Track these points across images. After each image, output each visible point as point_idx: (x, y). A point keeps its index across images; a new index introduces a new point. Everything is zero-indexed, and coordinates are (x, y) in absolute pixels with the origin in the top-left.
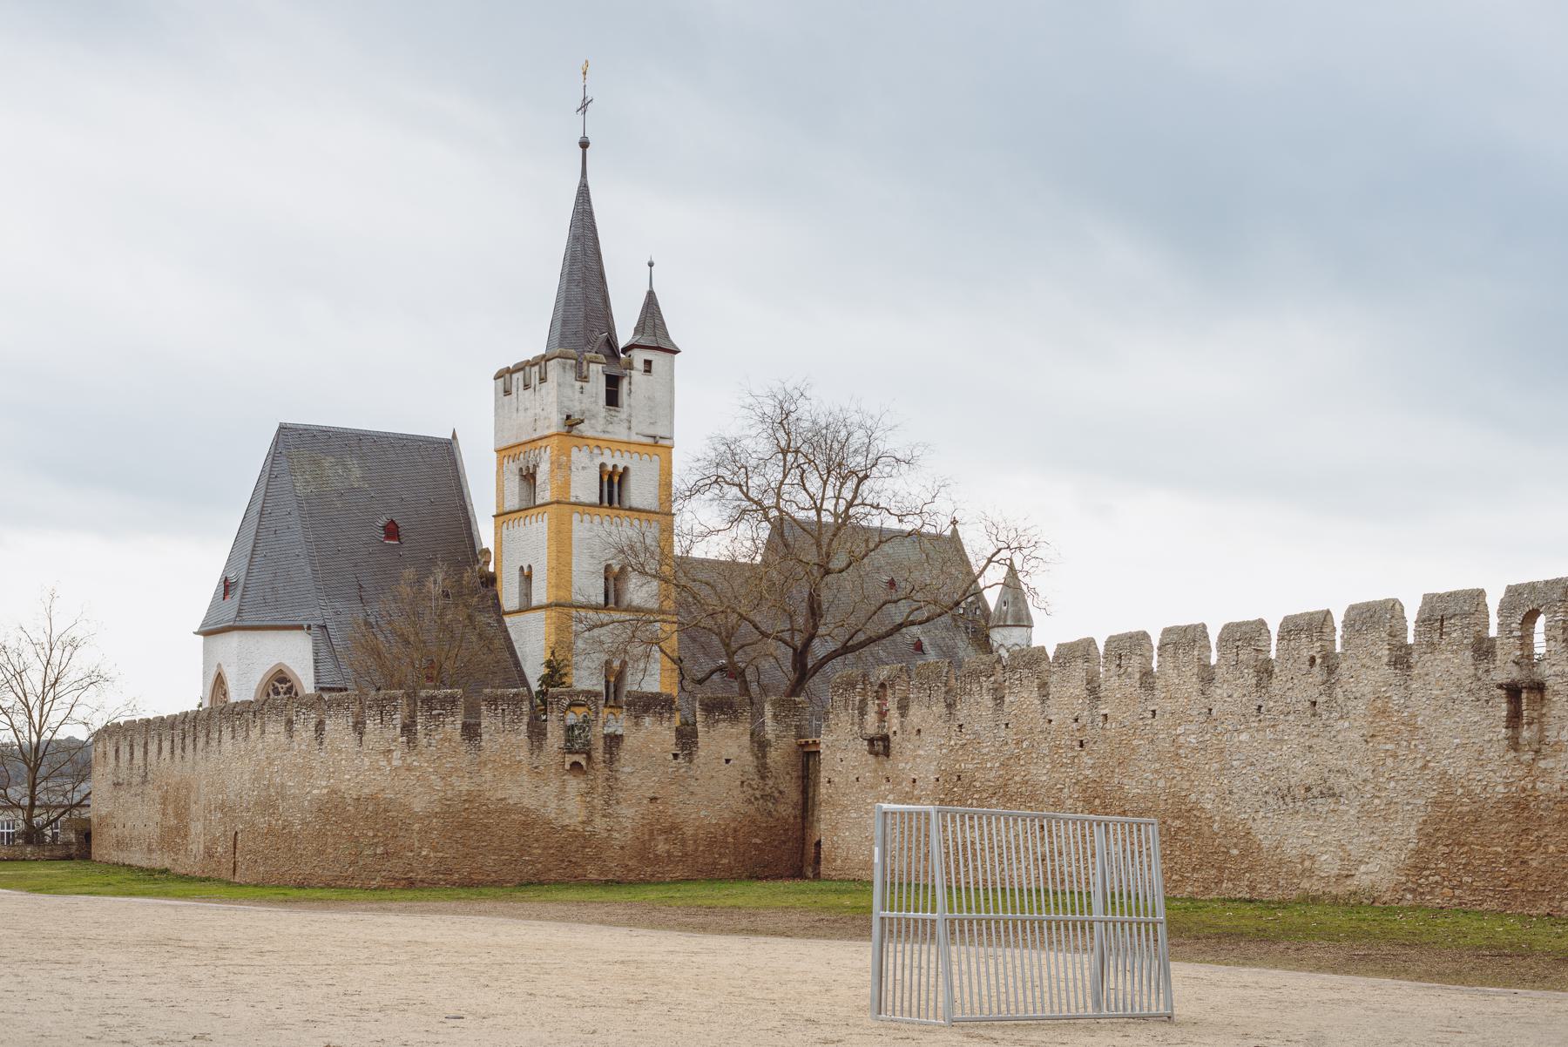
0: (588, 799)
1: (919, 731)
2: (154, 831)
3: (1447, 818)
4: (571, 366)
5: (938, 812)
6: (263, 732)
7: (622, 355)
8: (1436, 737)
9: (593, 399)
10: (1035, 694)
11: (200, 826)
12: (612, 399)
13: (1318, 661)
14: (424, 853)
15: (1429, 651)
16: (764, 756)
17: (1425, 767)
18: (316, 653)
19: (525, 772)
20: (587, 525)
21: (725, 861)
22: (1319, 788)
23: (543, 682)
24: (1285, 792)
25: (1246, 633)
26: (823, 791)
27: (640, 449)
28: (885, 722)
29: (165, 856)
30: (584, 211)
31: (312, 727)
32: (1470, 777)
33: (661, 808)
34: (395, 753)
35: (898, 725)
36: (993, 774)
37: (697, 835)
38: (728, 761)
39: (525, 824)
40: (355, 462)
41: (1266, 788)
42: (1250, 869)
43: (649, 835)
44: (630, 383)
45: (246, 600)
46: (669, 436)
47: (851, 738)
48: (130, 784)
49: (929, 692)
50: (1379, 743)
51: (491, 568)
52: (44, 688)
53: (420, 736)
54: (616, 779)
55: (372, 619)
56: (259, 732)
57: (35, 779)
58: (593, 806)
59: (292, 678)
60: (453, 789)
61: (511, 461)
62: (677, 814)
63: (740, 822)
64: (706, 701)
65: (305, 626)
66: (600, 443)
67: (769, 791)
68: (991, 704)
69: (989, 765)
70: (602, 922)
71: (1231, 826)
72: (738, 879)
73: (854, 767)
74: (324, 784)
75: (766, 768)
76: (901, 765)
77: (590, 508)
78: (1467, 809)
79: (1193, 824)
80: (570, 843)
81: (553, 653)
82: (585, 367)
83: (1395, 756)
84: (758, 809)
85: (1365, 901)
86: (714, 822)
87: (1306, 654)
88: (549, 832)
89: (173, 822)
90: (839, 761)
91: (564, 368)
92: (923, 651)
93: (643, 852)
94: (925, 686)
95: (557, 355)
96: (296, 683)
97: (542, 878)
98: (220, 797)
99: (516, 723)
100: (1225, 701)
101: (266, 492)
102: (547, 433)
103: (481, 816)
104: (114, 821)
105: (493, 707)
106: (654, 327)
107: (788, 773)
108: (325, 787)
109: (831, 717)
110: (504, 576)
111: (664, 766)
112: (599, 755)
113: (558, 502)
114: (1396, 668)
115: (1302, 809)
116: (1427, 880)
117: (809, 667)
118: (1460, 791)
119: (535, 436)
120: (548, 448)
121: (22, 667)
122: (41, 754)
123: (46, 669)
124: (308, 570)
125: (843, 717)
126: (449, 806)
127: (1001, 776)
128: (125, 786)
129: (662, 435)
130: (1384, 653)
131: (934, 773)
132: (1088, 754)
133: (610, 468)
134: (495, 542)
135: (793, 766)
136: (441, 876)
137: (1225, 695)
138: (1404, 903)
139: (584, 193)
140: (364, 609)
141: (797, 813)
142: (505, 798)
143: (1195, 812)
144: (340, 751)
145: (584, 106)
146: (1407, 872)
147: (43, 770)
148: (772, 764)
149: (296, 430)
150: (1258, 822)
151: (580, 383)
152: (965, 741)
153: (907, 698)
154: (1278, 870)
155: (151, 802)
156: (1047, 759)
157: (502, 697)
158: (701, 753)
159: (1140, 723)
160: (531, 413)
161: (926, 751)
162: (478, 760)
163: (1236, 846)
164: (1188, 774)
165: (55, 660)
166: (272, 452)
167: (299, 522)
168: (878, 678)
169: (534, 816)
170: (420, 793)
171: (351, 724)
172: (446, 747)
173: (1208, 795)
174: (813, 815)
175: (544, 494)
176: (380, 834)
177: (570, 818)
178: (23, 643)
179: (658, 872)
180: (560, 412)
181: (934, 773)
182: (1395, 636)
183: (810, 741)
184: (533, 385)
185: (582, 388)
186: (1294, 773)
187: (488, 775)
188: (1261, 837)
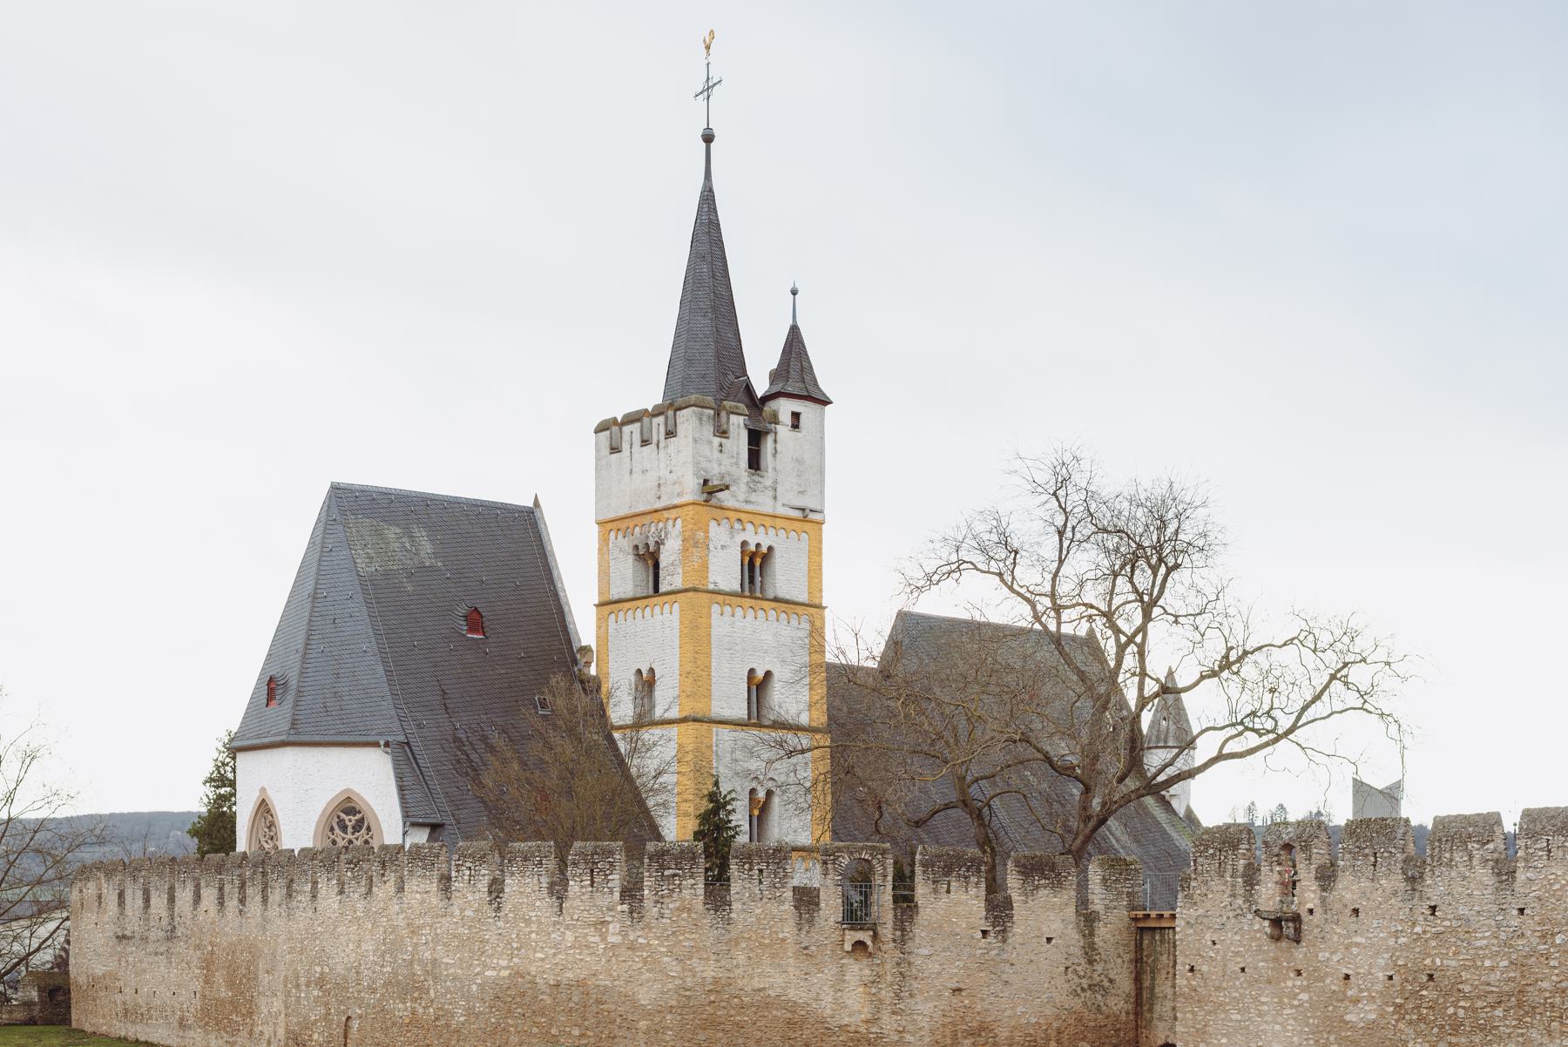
0: (874, 991)
1: (1356, 911)
9: (735, 460)
11: (277, 1005)
12: (755, 462)
16: (1092, 934)
18: (399, 778)
19: (791, 955)
20: (727, 618)
30: (710, 221)
31: (483, 885)
33: (967, 1002)
34: (611, 926)
35: (1317, 902)
37: (1012, 1038)
38: (1049, 940)
39: (790, 1023)
40: (424, 534)
44: (775, 441)
45: (302, 708)
46: (819, 508)
47: (1231, 914)
48: (145, 939)
51: (593, 671)
53: (648, 903)
54: (909, 964)
58: (880, 1000)
59: (364, 807)
63: (1064, 1020)
64: (1023, 861)
65: (382, 743)
66: (742, 516)
67: (1098, 979)
69: (1487, 963)
73: (1237, 954)
74: (504, 963)
75: (1095, 949)
77: (733, 598)
84: (1085, 1004)
86: (1034, 1020)
88: (824, 1034)
90: (1209, 943)
91: (701, 420)
94: (1367, 851)
95: (692, 403)
96: (369, 820)
98: (318, 969)
99: (778, 888)
101: (319, 570)
102: (677, 501)
103: (732, 1012)
105: (747, 866)
106: (802, 371)
107: (1119, 956)
108: (505, 968)
112: (887, 931)
119: (658, 505)
120: (679, 522)
124: (380, 670)
126: (689, 998)
128: (136, 941)
129: (813, 507)
131: (1384, 969)
139: (708, 199)
140: (450, 721)
141: (1130, 1008)
142: (764, 988)
144: (528, 922)
148: (1101, 944)
149: (351, 491)
151: (719, 439)
152: (1441, 929)
158: (1017, 930)
162: (727, 937)
166: (323, 519)
167: (364, 609)
169: (803, 1013)
170: (648, 981)
171: (545, 885)
172: (683, 919)
174: (1151, 1010)
176: (589, 1033)
177: (850, 1016)
180: (696, 475)
181: (1384, 969)
184: (655, 440)
185: (721, 445)
187: (741, 958)
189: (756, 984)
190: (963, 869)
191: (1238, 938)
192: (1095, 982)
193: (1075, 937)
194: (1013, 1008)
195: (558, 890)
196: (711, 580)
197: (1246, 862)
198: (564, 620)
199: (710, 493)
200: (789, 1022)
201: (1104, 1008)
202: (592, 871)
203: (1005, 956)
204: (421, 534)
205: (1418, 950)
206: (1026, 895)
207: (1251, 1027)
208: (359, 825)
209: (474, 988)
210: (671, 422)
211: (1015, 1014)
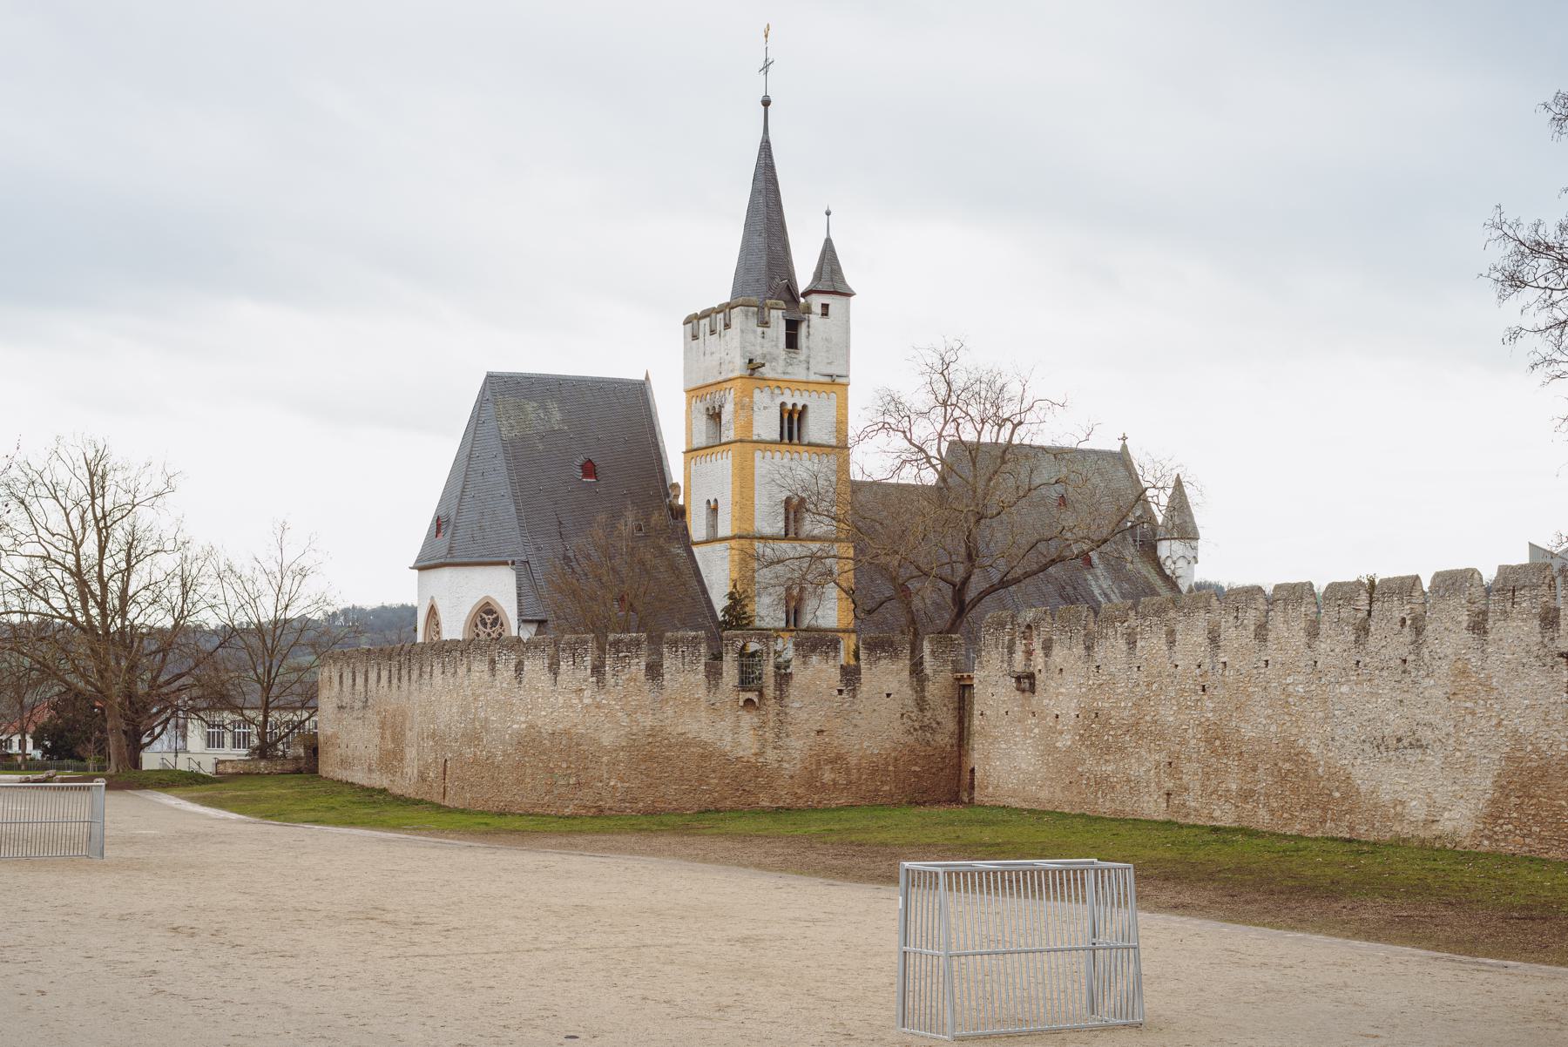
0: (760, 733)
1: (1061, 670)
2: (374, 753)
3: (1518, 772)
4: (753, 313)
5: (944, 873)
6: (469, 670)
7: (802, 300)
8: (1508, 698)
9: (774, 343)
10: (1163, 641)
12: (792, 342)
13: (1408, 622)
14: (612, 784)
15: (1503, 618)
16: (923, 690)
17: (1499, 724)
18: (519, 587)
21: (886, 788)
22: (1409, 740)
23: (726, 612)
24: (1380, 742)
25: (1346, 593)
26: (976, 722)
27: (817, 387)
28: (1031, 660)
29: (384, 777)
30: (766, 164)
32: (1538, 735)
34: (585, 692)
35: (1043, 664)
36: (1126, 713)
38: (888, 695)
41: (1362, 738)
42: (1350, 811)
43: (817, 766)
44: (808, 326)
46: (844, 374)
48: (352, 708)
49: (1069, 634)
50: (1460, 701)
51: (681, 501)
52: (276, 612)
53: (608, 676)
54: (786, 714)
55: (571, 554)
56: (465, 670)
57: (268, 698)
59: (498, 609)
60: (638, 725)
61: (698, 402)
62: (842, 745)
65: (510, 562)
66: (781, 384)
67: (928, 722)
68: (1124, 647)
70: (758, 866)
71: (1333, 770)
72: (898, 805)
74: (523, 719)
75: (925, 701)
76: (1046, 702)
78: (1536, 764)
79: (1301, 767)
80: (744, 773)
81: (735, 586)
82: (766, 313)
83: (1473, 713)
84: (917, 740)
85: (1448, 845)
86: (876, 752)
87: (1398, 615)
89: (391, 746)
91: (746, 316)
92: (1091, 566)
93: (811, 780)
94: (1067, 629)
96: (502, 617)
97: (719, 806)
98: (432, 726)
100: (1328, 655)
102: (731, 376)
103: (664, 749)
104: (339, 741)
105: (674, 649)
107: (945, 705)
108: (524, 722)
109: (983, 654)
110: (692, 508)
111: (830, 701)
112: (770, 691)
113: (741, 441)
114: (1474, 633)
115: (1395, 758)
116: (1501, 828)
117: (967, 602)
118: (1530, 748)
119: (720, 378)
121: (257, 595)
122: (273, 675)
123: (278, 596)
124: (513, 509)
125: (994, 654)
126: (635, 740)
127: (1133, 715)
128: (347, 710)
129: (839, 374)
130: (1464, 618)
132: (1209, 698)
133: (790, 407)
134: (685, 476)
135: (949, 698)
136: (627, 805)
137: (1328, 649)
138: (1481, 849)
139: (766, 148)
143: (1302, 756)
145: (766, 67)
146: (1484, 820)
147: (275, 690)
150: (1357, 768)
153: (1050, 640)
154: (1374, 813)
155: (371, 726)
156: (1173, 701)
157: (682, 639)
158: (864, 688)
159: (1255, 671)
160: (716, 357)
161: (1067, 689)
162: (660, 698)
163: (1338, 789)
164: (1297, 721)
165: (286, 588)
167: (504, 464)
168: (1025, 620)
169: (711, 749)
173: (1313, 741)
174: (968, 743)
175: (729, 434)
177: (744, 751)
178: (257, 572)
179: (825, 799)
180: (743, 356)
182: (1474, 603)
183: (965, 675)
184: (718, 332)
186: (1387, 724)
187: (670, 712)
188: (1359, 782)
189: (680, 730)
190: (825, 647)
191: (1004, 691)
192: (925, 724)
193: (908, 692)
194: (861, 744)
195: (554, 669)
196: (755, 432)
197: (1010, 637)
198: (662, 464)
199: (753, 369)
200: (702, 756)
201: (932, 743)
202: (574, 655)
203: (855, 707)
204: (554, 407)
205: (1090, 696)
206: (871, 664)
207: (1011, 753)
208: (494, 623)
209: (507, 736)
210: (696, 327)
211: (862, 748)
